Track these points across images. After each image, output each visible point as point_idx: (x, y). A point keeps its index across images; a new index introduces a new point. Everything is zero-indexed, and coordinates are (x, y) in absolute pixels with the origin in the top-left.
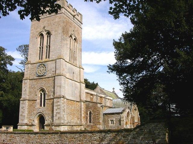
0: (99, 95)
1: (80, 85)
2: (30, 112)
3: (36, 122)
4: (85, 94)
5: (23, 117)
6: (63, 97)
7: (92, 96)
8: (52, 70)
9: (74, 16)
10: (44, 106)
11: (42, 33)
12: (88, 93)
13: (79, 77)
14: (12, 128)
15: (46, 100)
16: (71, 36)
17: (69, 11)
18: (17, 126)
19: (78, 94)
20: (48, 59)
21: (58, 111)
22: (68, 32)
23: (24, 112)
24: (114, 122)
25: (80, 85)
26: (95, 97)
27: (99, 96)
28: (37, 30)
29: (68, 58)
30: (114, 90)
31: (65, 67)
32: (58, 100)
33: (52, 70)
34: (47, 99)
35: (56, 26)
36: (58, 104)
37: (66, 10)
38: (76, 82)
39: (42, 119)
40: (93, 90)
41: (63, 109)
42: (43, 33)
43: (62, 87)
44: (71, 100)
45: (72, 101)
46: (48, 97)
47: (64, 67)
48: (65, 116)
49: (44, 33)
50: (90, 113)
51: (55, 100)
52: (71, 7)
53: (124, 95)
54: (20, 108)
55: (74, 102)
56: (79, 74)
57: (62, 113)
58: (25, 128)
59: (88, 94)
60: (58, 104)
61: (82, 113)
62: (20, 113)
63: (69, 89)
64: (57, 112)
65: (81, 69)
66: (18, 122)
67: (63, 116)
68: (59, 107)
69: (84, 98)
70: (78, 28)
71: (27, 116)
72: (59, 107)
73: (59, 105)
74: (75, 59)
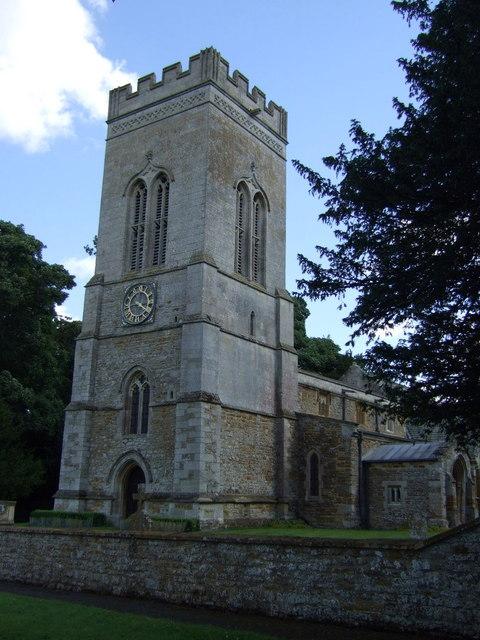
0: (354, 395)
1: (279, 359)
2: (91, 454)
3: (113, 487)
4: (296, 388)
5: (72, 468)
6: (211, 399)
7: (323, 400)
8: (173, 304)
9: (253, 114)
10: (145, 430)
11: (140, 177)
12: (306, 387)
13: (272, 330)
14: (12, 510)
15: (151, 410)
16: (242, 186)
17: (233, 95)
18: (53, 499)
19: (270, 390)
20: (155, 270)
21: (188, 450)
22: (229, 170)
23: (75, 452)
24: (404, 494)
25: (279, 359)
26: (336, 401)
27: (354, 399)
28: (126, 168)
29: (231, 262)
30: (350, 339)
31: (222, 293)
32: (189, 411)
33: (173, 304)
34: (92, 394)
35: (187, 149)
36: (191, 423)
37: (223, 91)
38: (262, 348)
39: (133, 476)
40: (337, 379)
41: (209, 441)
42: (144, 178)
43: (204, 364)
44: (242, 411)
45: (248, 415)
46: (154, 404)
47: (215, 291)
48: (216, 467)
49: (148, 178)
50: (314, 458)
51: (180, 410)
52: (240, 82)
53: (61, 101)
54: (65, 438)
55: (253, 417)
56: (273, 317)
57: (205, 458)
58: (74, 505)
59: (310, 392)
60: (191, 423)
61: (285, 459)
62: (65, 455)
63: (234, 371)
64: (184, 451)
65: (281, 300)
66: (55, 487)
67: (208, 468)
68: (192, 434)
69: (293, 403)
70: (271, 158)
71: (83, 464)
72: (192, 434)
73: (194, 428)
74: (260, 268)
